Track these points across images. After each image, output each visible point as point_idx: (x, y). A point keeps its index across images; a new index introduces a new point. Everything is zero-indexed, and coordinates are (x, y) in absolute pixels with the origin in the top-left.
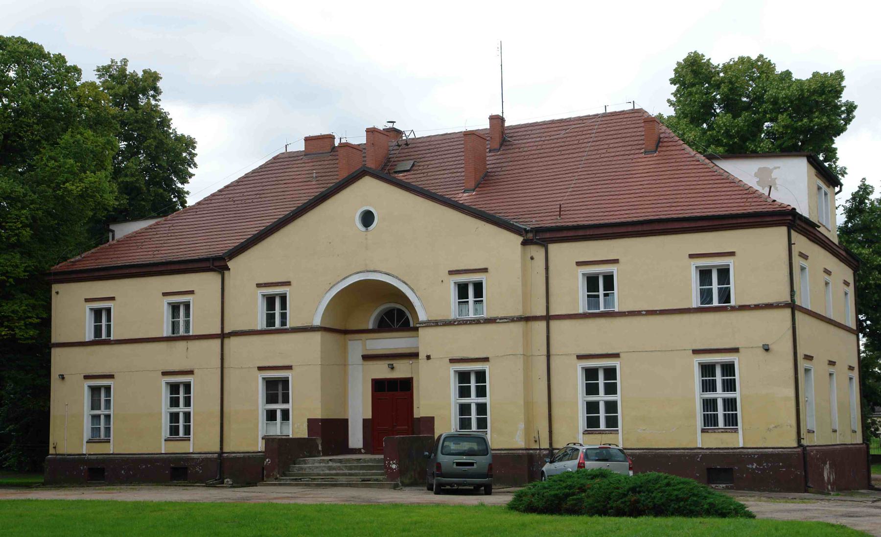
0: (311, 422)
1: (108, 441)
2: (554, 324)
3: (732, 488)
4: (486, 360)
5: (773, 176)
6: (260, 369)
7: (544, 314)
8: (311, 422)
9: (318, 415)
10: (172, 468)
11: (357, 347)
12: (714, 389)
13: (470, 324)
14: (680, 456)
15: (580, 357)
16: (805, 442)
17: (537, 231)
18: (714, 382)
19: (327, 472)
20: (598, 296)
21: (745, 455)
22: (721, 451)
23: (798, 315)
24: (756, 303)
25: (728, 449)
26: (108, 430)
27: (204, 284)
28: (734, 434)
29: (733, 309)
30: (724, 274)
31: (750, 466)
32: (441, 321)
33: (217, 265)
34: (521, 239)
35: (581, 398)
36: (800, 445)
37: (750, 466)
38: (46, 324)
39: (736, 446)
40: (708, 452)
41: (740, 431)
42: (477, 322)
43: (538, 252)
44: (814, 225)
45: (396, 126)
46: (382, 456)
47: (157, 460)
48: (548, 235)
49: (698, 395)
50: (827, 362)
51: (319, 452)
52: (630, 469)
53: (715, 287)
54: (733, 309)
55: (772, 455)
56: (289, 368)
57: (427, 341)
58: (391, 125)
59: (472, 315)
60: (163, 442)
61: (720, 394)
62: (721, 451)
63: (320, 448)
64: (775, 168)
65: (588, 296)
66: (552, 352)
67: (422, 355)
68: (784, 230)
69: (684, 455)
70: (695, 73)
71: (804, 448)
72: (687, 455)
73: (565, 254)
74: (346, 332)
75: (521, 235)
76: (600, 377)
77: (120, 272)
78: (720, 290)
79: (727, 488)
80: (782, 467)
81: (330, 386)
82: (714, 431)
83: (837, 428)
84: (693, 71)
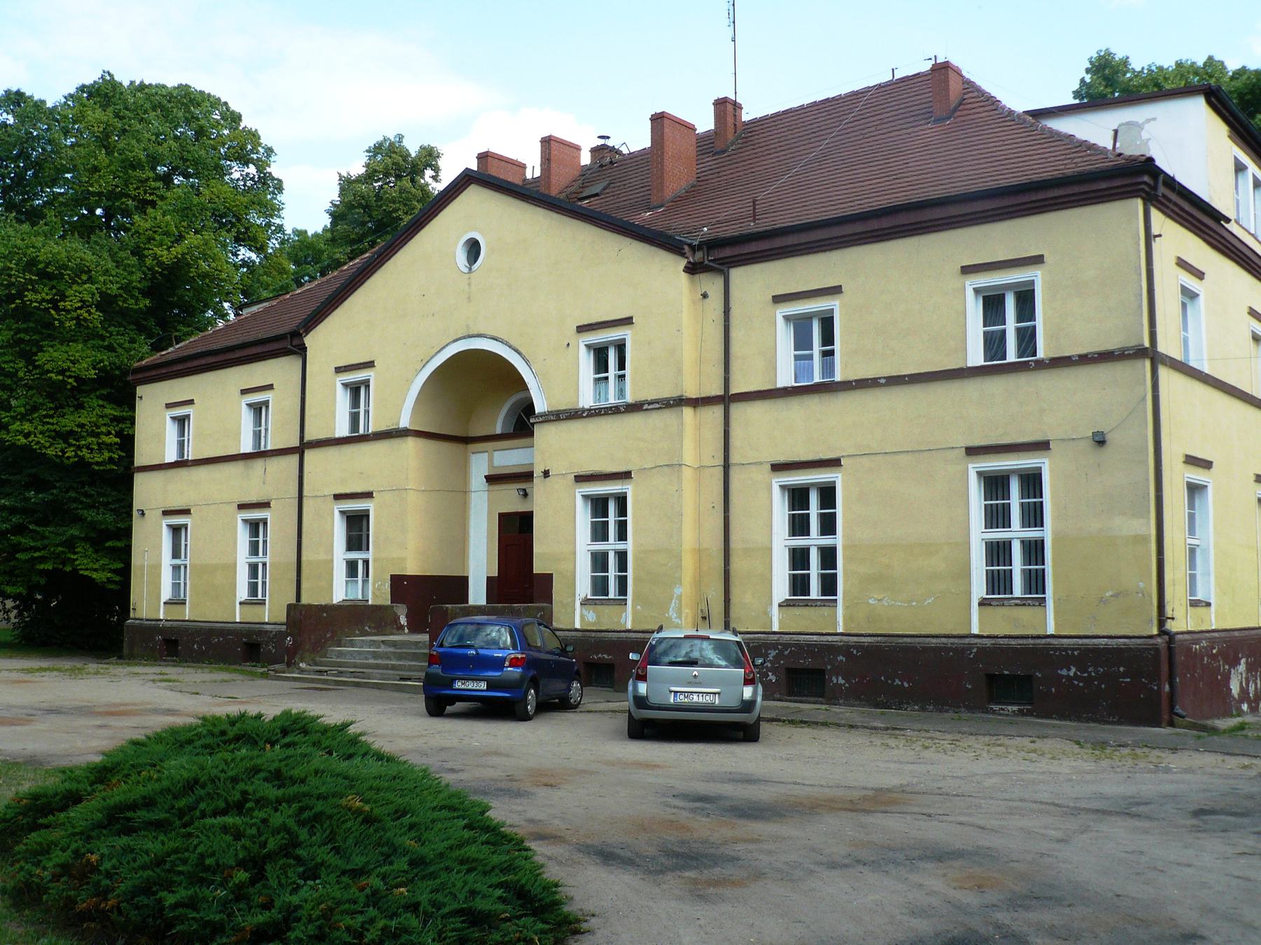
0: (397, 581)
1: (262, 603)
2: (737, 410)
3: (1030, 713)
4: (626, 475)
5: (1145, 135)
6: (338, 497)
7: (720, 392)
8: (397, 581)
9: (412, 568)
10: (245, 643)
11: (480, 464)
12: (1006, 523)
13: (606, 414)
14: (937, 650)
15: (778, 468)
16: (1173, 626)
17: (712, 245)
18: (1006, 509)
19: (372, 661)
20: (810, 357)
21: (1055, 649)
22: (1013, 642)
23: (1163, 372)
24: (1083, 351)
25: (1026, 637)
26: (622, 582)
27: (279, 372)
28: (1038, 610)
29: (1041, 365)
30: (1026, 299)
31: (1064, 672)
32: (565, 411)
33: (290, 344)
34: (683, 263)
35: (781, 541)
36: (1163, 632)
37: (1064, 672)
38: (127, 443)
39: (1041, 633)
40: (988, 642)
41: (1050, 603)
42: (614, 411)
43: (713, 284)
44: (1218, 217)
45: (610, 143)
46: (426, 637)
47: (230, 632)
48: (727, 252)
49: (979, 535)
50: (1253, 478)
51: (402, 627)
52: (748, 682)
53: (1011, 325)
54: (1041, 365)
55: (1107, 651)
56: (368, 495)
57: (552, 448)
58: (602, 142)
59: (612, 400)
60: (238, 606)
61: (1016, 532)
62: (1013, 642)
63: (403, 621)
64: (1148, 121)
65: (797, 358)
66: (735, 458)
67: (538, 473)
68: (1139, 203)
69: (945, 649)
70: (1110, 81)
71: (1171, 636)
72: (950, 649)
73: (754, 283)
74: (466, 440)
75: (683, 255)
76: (810, 503)
77: (203, 361)
78: (1019, 331)
79: (1021, 713)
80: (1124, 675)
81: (424, 521)
82: (1001, 603)
83: (1212, 601)
84: (1106, 78)
